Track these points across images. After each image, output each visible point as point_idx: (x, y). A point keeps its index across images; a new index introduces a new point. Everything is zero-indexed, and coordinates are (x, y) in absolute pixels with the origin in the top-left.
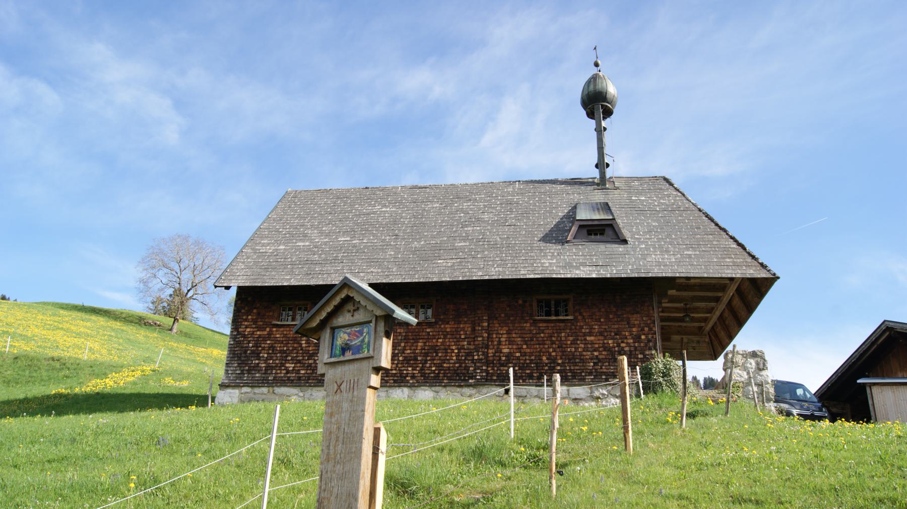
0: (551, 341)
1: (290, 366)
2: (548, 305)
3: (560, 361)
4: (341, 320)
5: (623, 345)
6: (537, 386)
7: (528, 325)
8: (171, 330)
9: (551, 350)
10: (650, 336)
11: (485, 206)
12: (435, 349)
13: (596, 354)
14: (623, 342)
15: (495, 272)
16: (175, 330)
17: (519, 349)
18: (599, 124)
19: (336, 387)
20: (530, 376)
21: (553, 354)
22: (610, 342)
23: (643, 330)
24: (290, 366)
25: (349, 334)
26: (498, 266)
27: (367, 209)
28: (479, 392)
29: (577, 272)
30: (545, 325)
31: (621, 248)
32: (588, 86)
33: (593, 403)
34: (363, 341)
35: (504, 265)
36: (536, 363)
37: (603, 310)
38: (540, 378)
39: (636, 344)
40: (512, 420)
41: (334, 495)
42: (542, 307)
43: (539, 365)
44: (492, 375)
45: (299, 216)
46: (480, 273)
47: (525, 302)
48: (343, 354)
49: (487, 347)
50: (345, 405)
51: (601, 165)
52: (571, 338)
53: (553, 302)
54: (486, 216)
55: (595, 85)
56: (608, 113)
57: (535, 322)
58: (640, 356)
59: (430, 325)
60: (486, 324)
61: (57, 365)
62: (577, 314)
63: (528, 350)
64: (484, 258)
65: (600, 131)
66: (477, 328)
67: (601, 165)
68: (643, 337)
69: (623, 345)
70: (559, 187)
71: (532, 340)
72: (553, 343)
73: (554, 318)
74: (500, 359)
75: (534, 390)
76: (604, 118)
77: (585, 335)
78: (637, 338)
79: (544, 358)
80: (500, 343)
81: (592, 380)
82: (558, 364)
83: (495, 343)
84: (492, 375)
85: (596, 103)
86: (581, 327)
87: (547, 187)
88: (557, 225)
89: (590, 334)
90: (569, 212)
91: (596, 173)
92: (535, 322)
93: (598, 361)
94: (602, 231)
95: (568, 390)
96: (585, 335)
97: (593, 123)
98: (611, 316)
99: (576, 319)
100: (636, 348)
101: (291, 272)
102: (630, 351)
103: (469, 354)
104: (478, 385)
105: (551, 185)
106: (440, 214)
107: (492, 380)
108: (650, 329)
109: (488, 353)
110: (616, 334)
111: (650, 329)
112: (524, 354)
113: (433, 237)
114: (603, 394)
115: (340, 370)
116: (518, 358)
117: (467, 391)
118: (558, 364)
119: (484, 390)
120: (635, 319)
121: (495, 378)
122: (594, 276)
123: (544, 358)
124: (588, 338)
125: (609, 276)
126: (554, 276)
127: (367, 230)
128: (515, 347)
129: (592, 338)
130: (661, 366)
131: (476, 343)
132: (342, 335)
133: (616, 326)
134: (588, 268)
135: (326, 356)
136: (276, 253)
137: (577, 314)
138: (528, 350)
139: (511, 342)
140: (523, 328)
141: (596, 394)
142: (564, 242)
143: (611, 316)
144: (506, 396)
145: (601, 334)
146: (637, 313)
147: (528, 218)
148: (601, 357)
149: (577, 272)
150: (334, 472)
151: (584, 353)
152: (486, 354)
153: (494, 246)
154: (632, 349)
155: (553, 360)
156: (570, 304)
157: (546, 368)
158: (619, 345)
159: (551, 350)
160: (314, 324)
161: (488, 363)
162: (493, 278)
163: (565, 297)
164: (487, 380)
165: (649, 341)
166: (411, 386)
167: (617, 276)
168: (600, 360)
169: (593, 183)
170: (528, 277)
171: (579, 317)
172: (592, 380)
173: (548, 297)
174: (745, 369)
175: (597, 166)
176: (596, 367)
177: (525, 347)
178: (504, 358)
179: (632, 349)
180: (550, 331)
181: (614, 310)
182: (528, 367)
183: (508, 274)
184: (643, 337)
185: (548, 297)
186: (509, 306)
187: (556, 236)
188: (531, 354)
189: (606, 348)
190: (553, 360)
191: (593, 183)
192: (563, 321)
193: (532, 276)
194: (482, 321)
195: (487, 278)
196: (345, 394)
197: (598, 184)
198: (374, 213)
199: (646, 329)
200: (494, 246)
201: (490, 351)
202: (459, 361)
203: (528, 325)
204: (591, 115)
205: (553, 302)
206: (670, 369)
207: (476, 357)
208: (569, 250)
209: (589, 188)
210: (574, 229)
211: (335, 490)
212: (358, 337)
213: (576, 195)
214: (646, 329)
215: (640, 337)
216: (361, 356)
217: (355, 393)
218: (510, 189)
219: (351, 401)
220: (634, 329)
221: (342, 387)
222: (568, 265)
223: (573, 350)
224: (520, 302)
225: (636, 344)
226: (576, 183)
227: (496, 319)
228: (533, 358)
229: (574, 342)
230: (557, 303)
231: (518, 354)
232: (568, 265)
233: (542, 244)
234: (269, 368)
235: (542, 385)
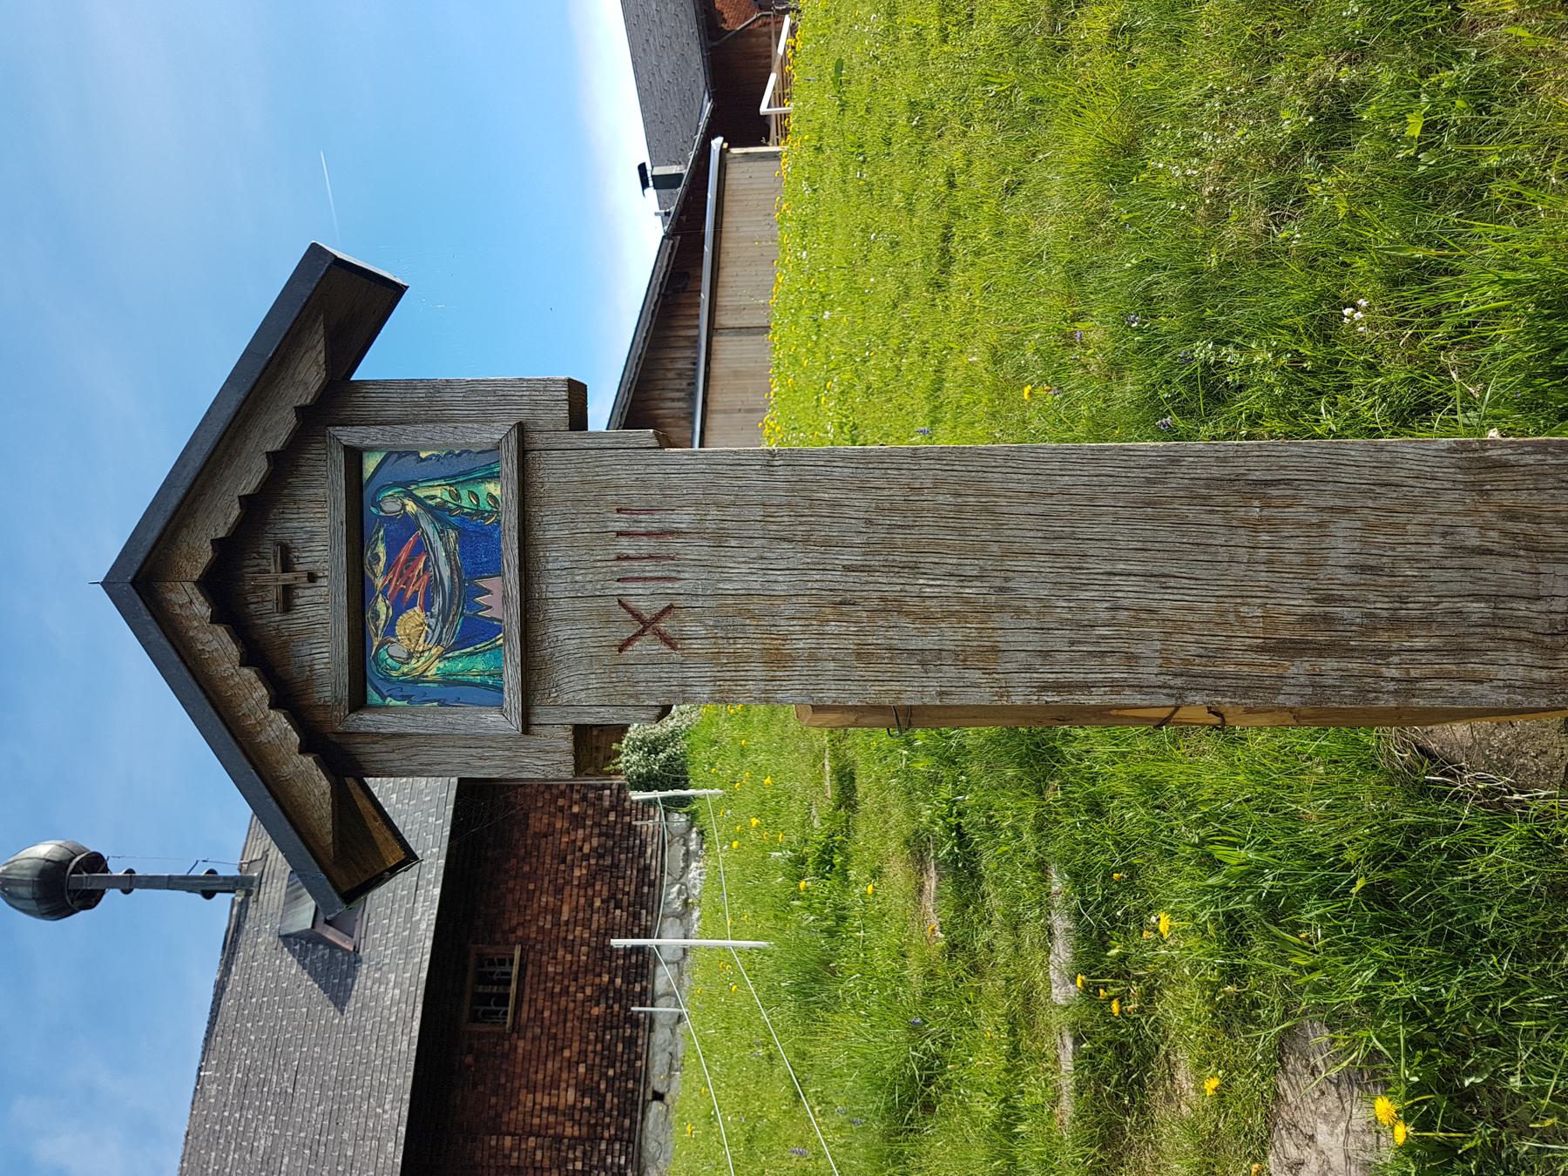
0: (560, 994)
2: (483, 999)
3: (606, 978)
4: (323, 655)
5: (586, 849)
6: (651, 1029)
7: (521, 1043)
9: (580, 996)
10: (576, 796)
11: (239, 1147)
13: (597, 903)
14: (581, 849)
15: (394, 1112)
17: (571, 1065)
18: (116, 882)
19: (647, 646)
20: (631, 1042)
21: (588, 991)
22: (577, 873)
23: (561, 809)
25: (400, 605)
26: (382, 1106)
28: (655, 1161)
29: (423, 926)
30: (525, 1007)
32: (20, 898)
33: (696, 914)
34: (438, 513)
35: (382, 1089)
36: (605, 1028)
37: (511, 884)
38: (634, 1021)
39: (589, 823)
40: (730, 942)
41: (1156, 597)
42: (487, 1014)
43: (609, 1023)
44: (620, 1128)
46: (391, 1144)
47: (470, 1049)
48: (490, 629)
49: (559, 1139)
50: (740, 575)
51: (208, 887)
52: (561, 952)
53: (480, 989)
54: (262, 1144)
55: (21, 883)
56: (95, 862)
57: (517, 1028)
58: (612, 817)
60: (508, 1140)
62: (512, 938)
63: (576, 1046)
64: (356, 1140)
65: (130, 882)
66: (514, 1162)
67: (208, 887)
68: (576, 809)
69: (586, 849)
70: (234, 976)
71: (555, 1037)
72: (565, 991)
73: (514, 985)
74: (588, 1109)
75: (660, 1036)
76: (106, 870)
77: (557, 923)
78: (577, 821)
79: (595, 1011)
80: (552, 1109)
81: (650, 912)
82: (611, 981)
83: (552, 1119)
84: (620, 1128)
85: (66, 887)
86: (541, 930)
87: (228, 1002)
88: (315, 976)
89: (557, 912)
90: (293, 952)
91: (223, 901)
92: (517, 1028)
95: (663, 996)
96: (557, 923)
97: (112, 896)
98: (526, 869)
99: (523, 941)
100: (595, 825)
102: (600, 835)
105: (226, 996)
107: (631, 1130)
108: (562, 794)
109: (572, 1138)
110: (564, 861)
111: (562, 794)
112: (583, 1053)
114: (680, 892)
115: (567, 635)
116: (590, 1069)
118: (611, 981)
119: (651, 1147)
121: (627, 1122)
122: (437, 891)
123: (595, 1011)
124: (565, 917)
125: (442, 862)
126: (424, 975)
128: (565, 1076)
129: (566, 908)
130: (635, 758)
131: (546, 1163)
132: (398, 650)
133: (548, 861)
134: (419, 905)
135: (492, 718)
137: (512, 938)
138: (576, 1046)
139: (554, 1084)
140: (527, 1056)
141: (678, 905)
142: (354, 958)
143: (526, 869)
144: (668, 1099)
145: (559, 891)
146: (526, 816)
147: (288, 1043)
148: (605, 894)
149: (423, 926)
150: (1046, 605)
151: (594, 926)
152: (575, 1141)
153: (334, 1119)
154: (596, 831)
156: (490, 951)
157: (616, 1007)
158: (587, 857)
159: (580, 996)
160: (320, 785)
161: (594, 1139)
162: (405, 1113)
163: (472, 962)
164: (630, 1141)
165: (584, 798)
167: (445, 846)
168: (612, 896)
169: (244, 905)
170: (416, 1033)
171: (520, 933)
172: (650, 912)
173: (468, 997)
175: (209, 895)
176: (625, 903)
177: (567, 1053)
178: (587, 1101)
179: (596, 831)
180: (541, 995)
181: (514, 861)
182: (609, 1047)
183: (404, 1080)
184: (576, 809)
185: (468, 997)
186: (475, 1086)
187: (331, 964)
188: (584, 1040)
189: (589, 882)
191: (244, 905)
192: (523, 968)
193: (416, 1025)
194: (499, 1147)
195: (403, 1129)
196: (691, 579)
197: (248, 894)
199: (561, 802)
200: (334, 1119)
201: (568, 1131)
203: (521, 1043)
204: (90, 899)
205: (480, 989)
206: (643, 741)
207: (579, 1165)
208: (374, 947)
209: (251, 913)
210: (331, 934)
211: (1129, 592)
212: (421, 548)
213: (261, 939)
214: (561, 802)
215: (576, 815)
216: (510, 520)
217: (682, 520)
218: (213, 1089)
219: (719, 539)
220: (558, 825)
221: (647, 607)
222: (406, 948)
223: (584, 949)
224: (469, 1059)
225: (589, 823)
226: (234, 942)
227: (498, 1115)
228: (592, 1036)
229: (570, 947)
230: (484, 979)
231: (582, 1069)
232: (406, 948)
233: (351, 1005)
235: (651, 1018)
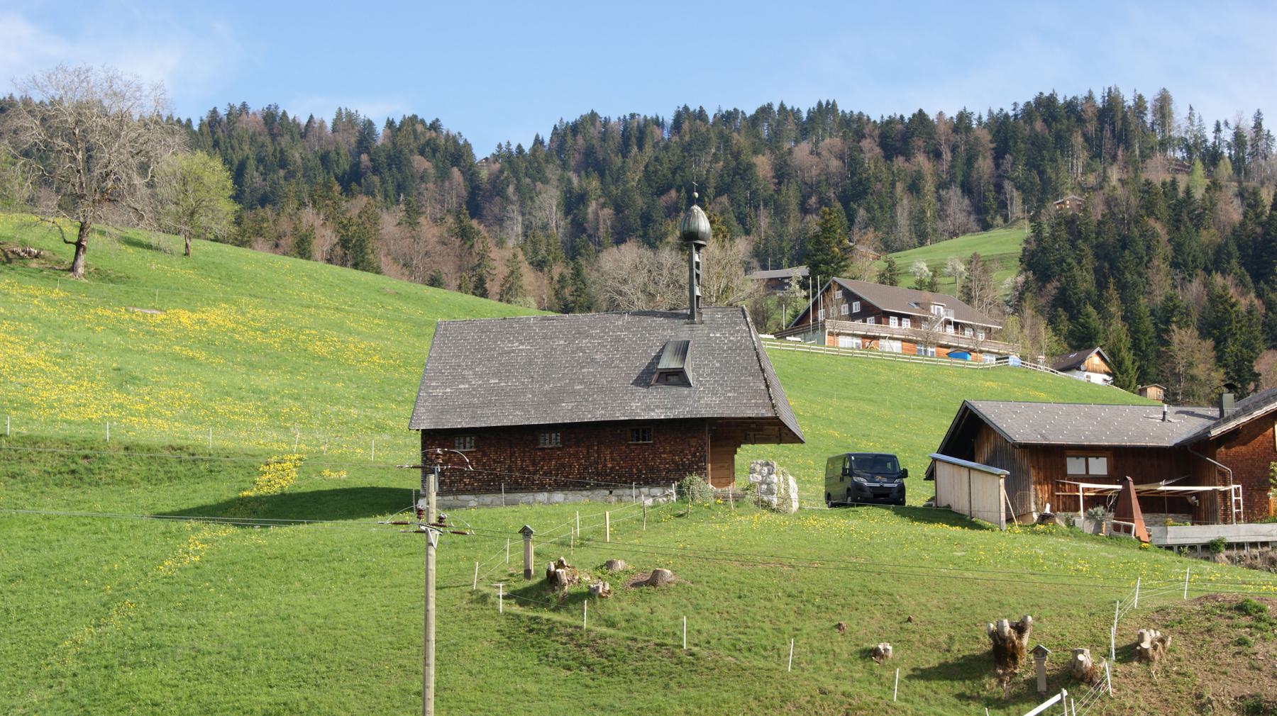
1: (467, 481)
2: (638, 431)
8: (72, 269)
12: (563, 466)
16: (81, 270)
20: (625, 482)
24: (467, 481)
27: (508, 346)
31: (685, 391)
43: (631, 475)
45: (455, 356)
59: (559, 449)
61: (185, 456)
75: (628, 491)
78: (694, 455)
93: (669, 471)
94: (676, 377)
101: (460, 416)
103: (586, 468)
104: (593, 488)
106: (565, 352)
113: (559, 379)
117: (585, 493)
120: (693, 442)
127: (509, 371)
136: (445, 397)
139: (613, 459)
142: (648, 385)
153: (601, 390)
155: (640, 471)
161: (598, 474)
166: (549, 491)
174: (760, 473)
189: (673, 461)
190: (640, 471)
198: (513, 351)
202: (579, 473)
209: (682, 321)
210: (656, 376)
230: (644, 432)
234: (452, 482)
